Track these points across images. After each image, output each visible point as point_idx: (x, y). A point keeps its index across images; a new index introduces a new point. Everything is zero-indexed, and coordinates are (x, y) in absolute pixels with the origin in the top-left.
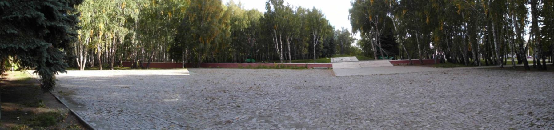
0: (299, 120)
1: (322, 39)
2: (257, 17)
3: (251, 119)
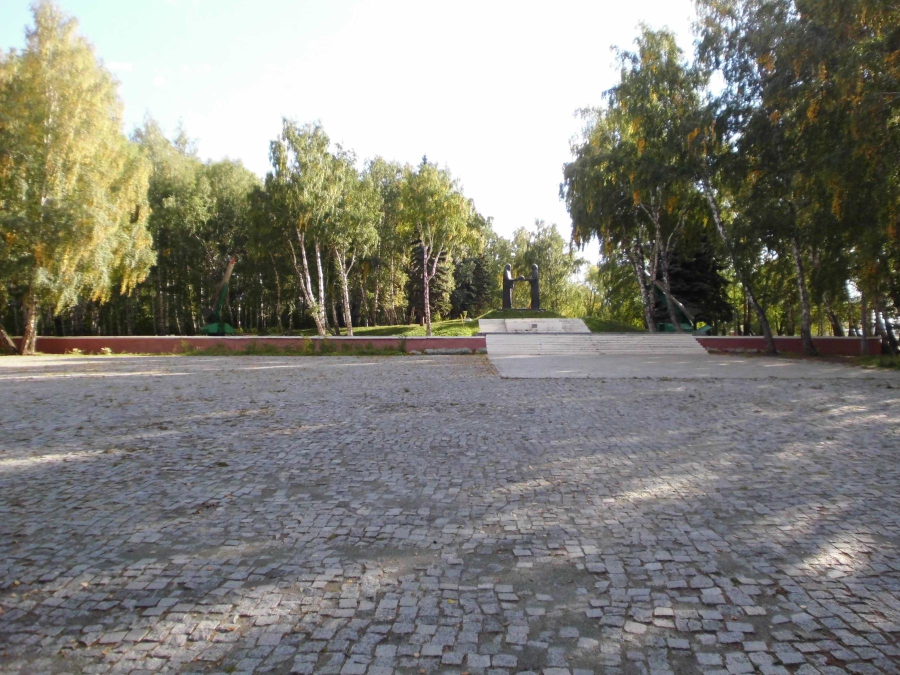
0: (404, 491)
1: (449, 258)
2: (240, 188)
3: (268, 493)
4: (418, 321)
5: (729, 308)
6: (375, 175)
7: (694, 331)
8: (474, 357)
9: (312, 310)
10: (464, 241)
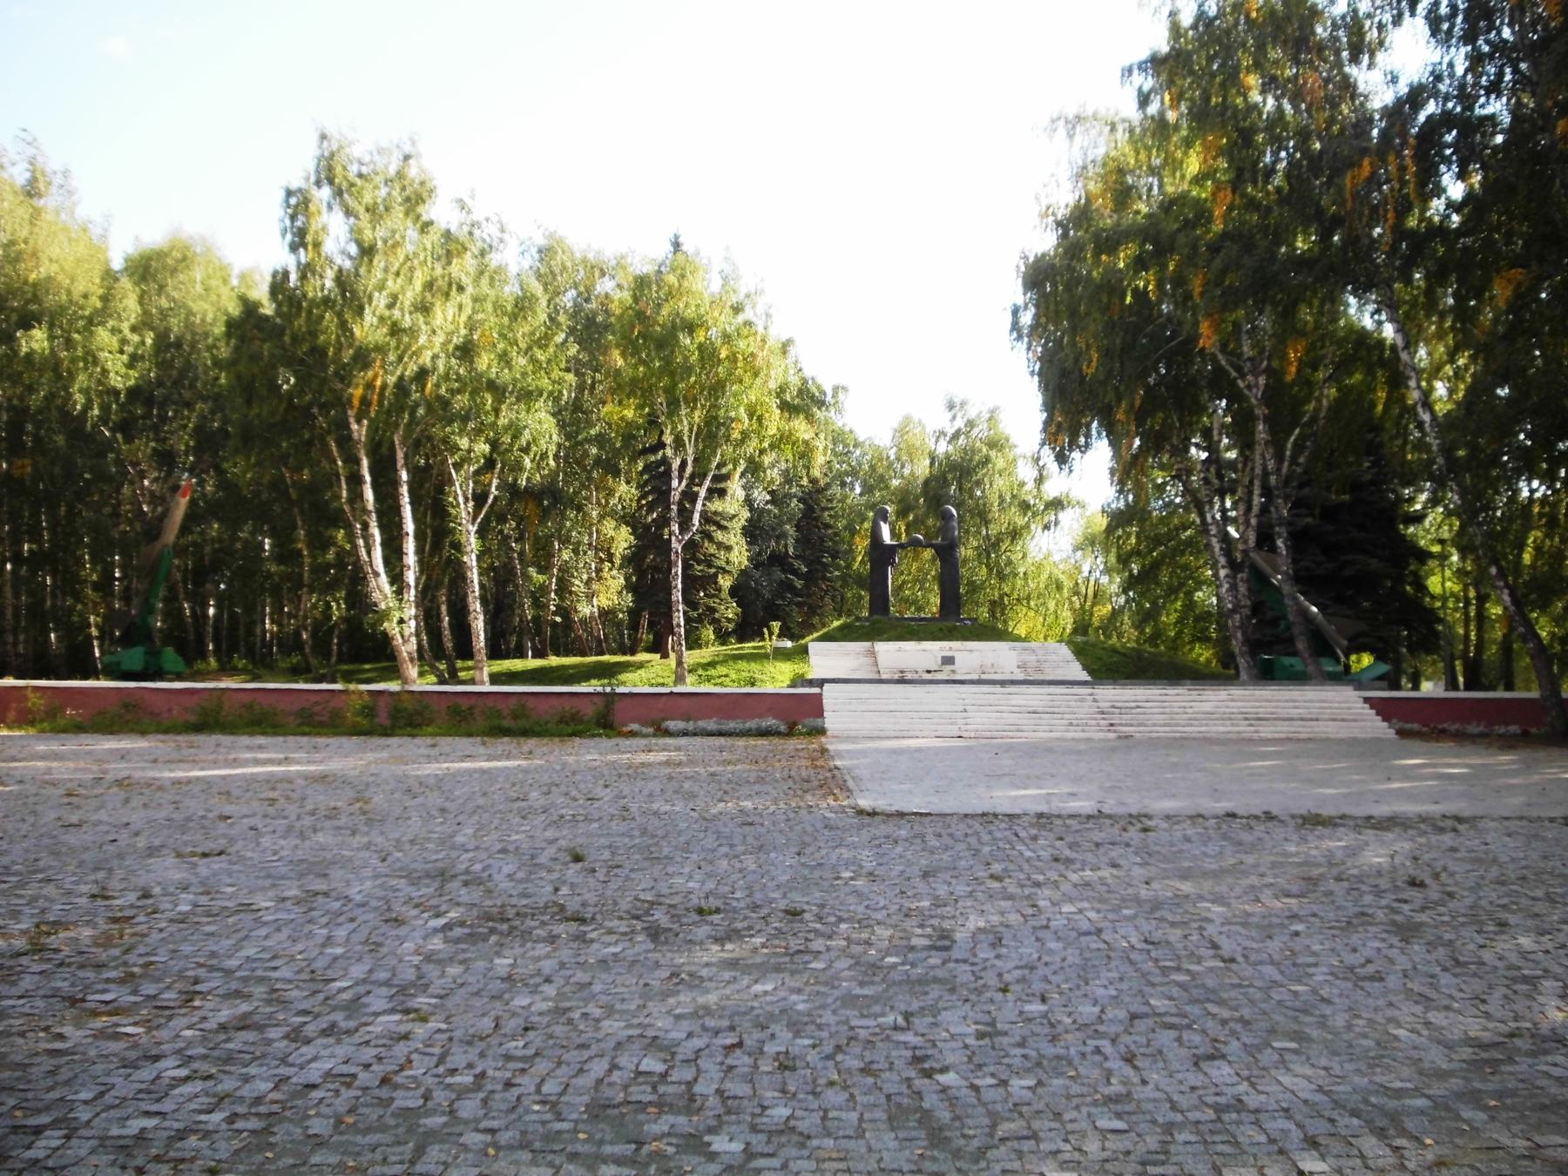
1: (735, 487)
2: (208, 306)
4: (658, 647)
5: (1431, 617)
6: (547, 278)
7: (1344, 676)
8: (792, 744)
9: (385, 615)
10: (772, 447)
